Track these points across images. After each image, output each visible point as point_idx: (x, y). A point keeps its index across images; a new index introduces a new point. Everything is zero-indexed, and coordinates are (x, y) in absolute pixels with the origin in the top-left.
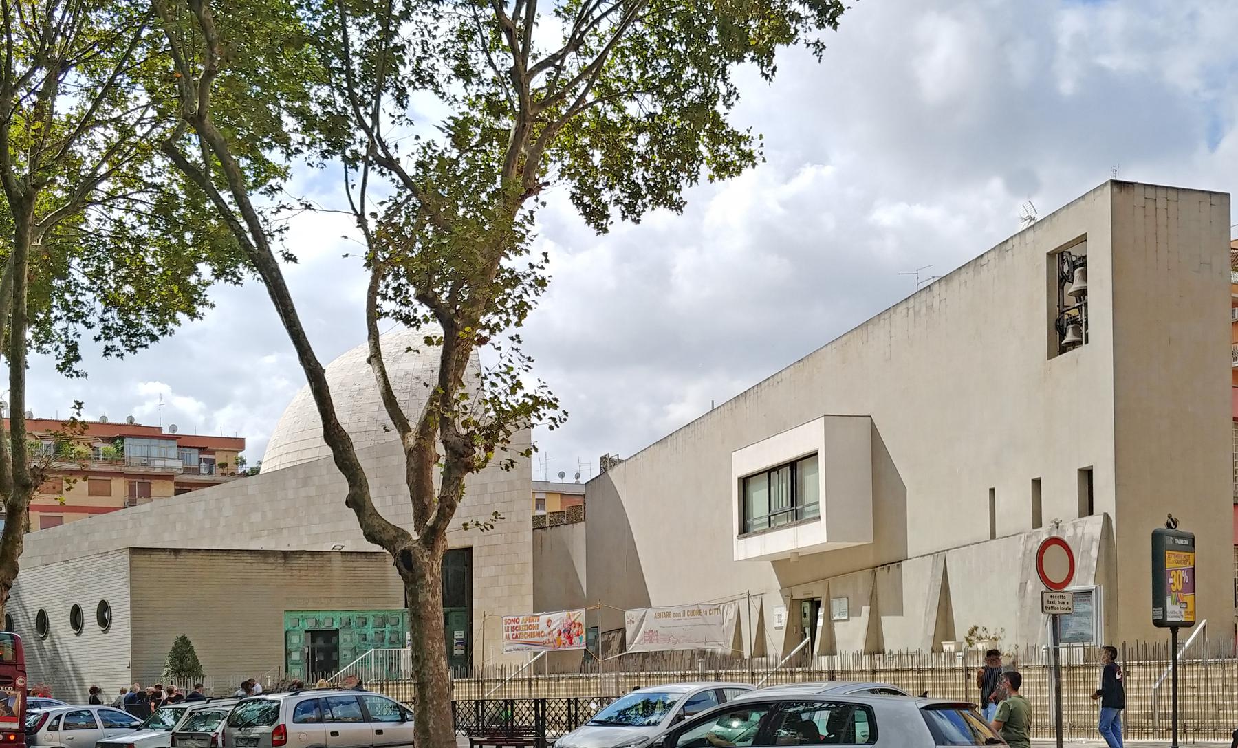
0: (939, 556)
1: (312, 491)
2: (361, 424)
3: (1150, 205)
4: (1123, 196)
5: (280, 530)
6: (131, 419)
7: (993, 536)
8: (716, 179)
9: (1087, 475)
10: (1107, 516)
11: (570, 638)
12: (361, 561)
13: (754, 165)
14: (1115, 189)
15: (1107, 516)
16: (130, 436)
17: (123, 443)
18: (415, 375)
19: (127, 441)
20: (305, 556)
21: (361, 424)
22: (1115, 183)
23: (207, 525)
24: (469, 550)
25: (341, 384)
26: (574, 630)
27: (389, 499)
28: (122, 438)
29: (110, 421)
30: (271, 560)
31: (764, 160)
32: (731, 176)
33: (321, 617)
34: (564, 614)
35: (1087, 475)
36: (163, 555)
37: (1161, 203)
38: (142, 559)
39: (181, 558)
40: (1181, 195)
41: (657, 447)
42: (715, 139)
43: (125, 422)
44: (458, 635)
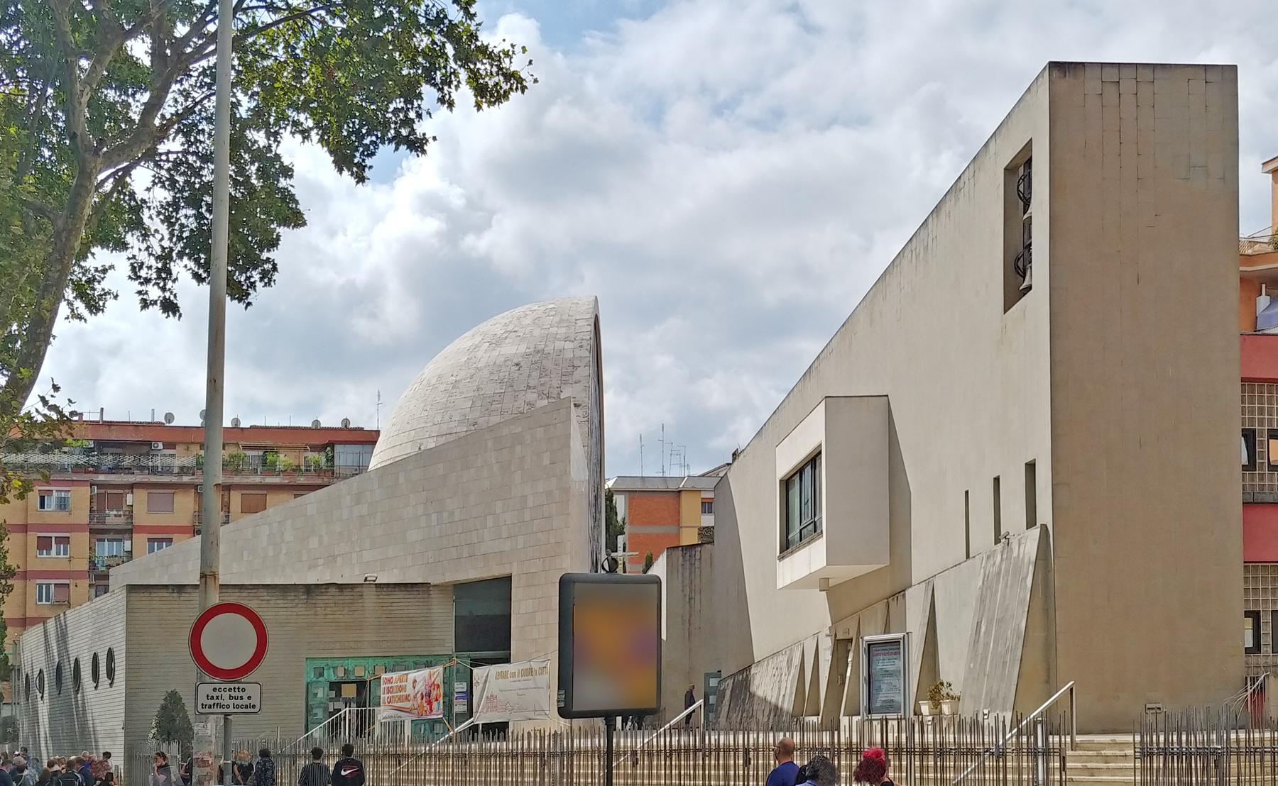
0: (929, 582)
1: (364, 509)
2: (452, 425)
3: (1111, 91)
4: (1064, 84)
5: (335, 557)
6: (346, 421)
7: (968, 557)
8: (485, 106)
9: (1031, 467)
10: (1044, 527)
11: (430, 703)
12: (399, 595)
13: (523, 89)
14: (1055, 73)
15: (1044, 527)
16: (341, 443)
17: (333, 450)
18: (516, 361)
19: (338, 448)
20: (332, 590)
21: (452, 425)
22: (1053, 66)
23: (271, 553)
24: (508, 579)
25: (440, 377)
26: (434, 694)
27: (434, 517)
28: (332, 444)
29: (323, 425)
30: (291, 596)
31: (536, 81)
32: (490, 104)
33: (350, 665)
34: (426, 672)
35: (1031, 467)
36: (164, 593)
37: (1127, 85)
38: (141, 599)
39: (185, 597)
40: (1159, 74)
41: (756, 441)
42: (465, 58)
43: (339, 425)
44: (460, 687)
